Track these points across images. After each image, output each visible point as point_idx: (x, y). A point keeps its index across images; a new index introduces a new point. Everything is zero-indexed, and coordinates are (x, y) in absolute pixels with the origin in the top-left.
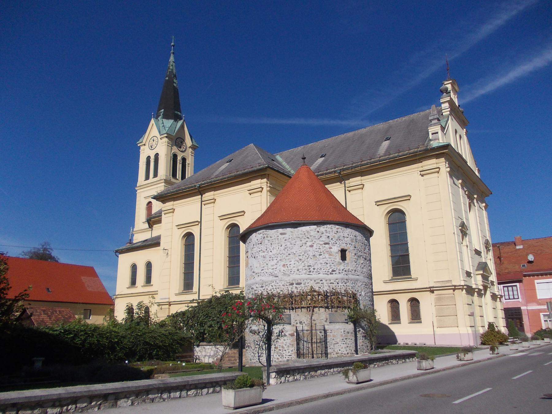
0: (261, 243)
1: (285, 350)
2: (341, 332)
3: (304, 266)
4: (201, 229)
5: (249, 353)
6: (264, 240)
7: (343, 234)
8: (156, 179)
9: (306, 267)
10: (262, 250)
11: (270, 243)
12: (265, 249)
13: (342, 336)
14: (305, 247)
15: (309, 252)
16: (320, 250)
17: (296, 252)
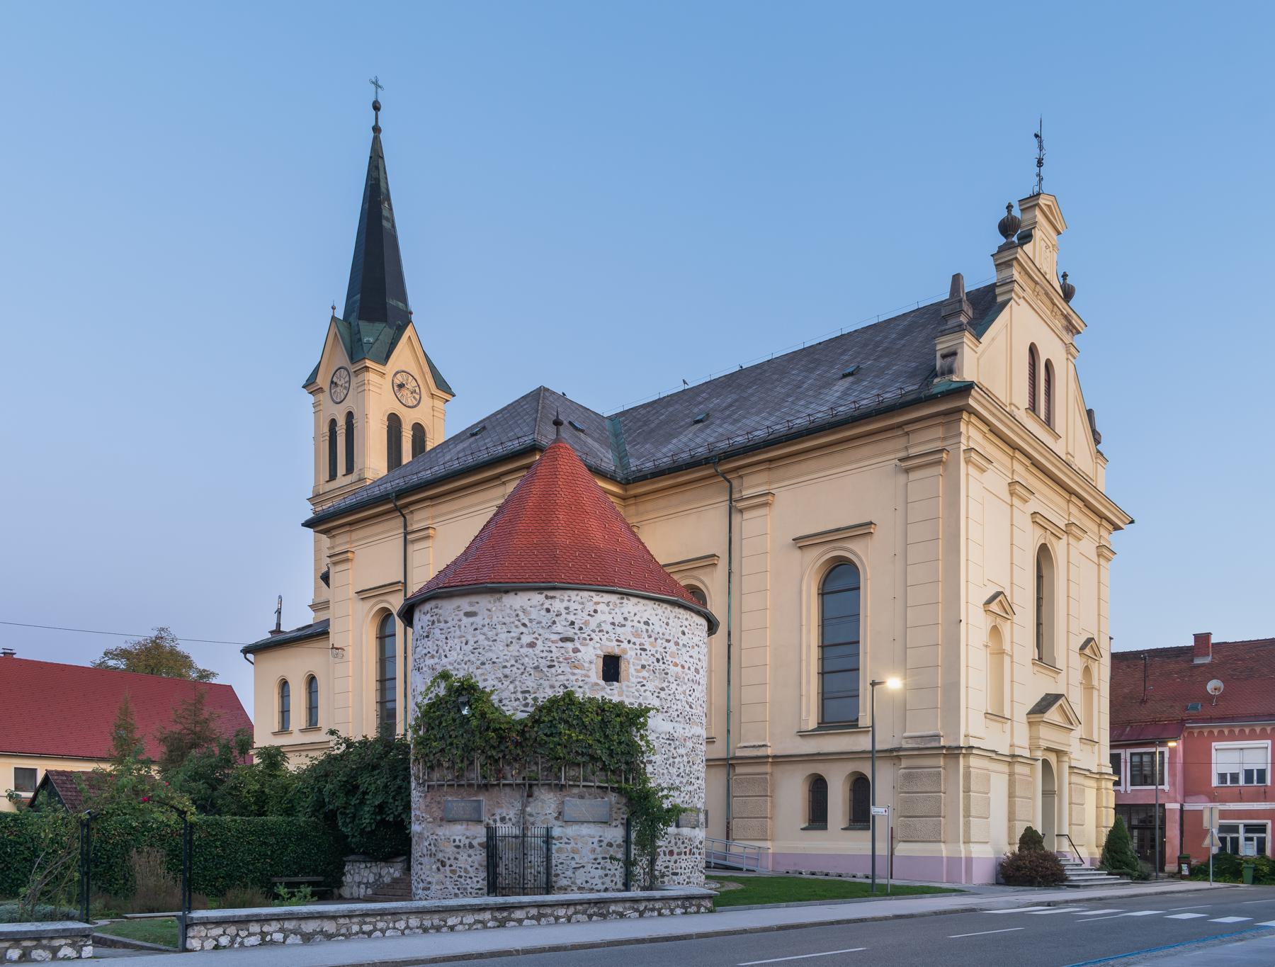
0: (427, 637)
1: (471, 878)
2: (593, 843)
3: (514, 693)
7: (612, 616)
8: (350, 479)
9: (520, 696)
11: (444, 636)
12: (434, 650)
13: (593, 851)
14: (518, 647)
15: (527, 659)
16: (549, 655)
17: (497, 658)
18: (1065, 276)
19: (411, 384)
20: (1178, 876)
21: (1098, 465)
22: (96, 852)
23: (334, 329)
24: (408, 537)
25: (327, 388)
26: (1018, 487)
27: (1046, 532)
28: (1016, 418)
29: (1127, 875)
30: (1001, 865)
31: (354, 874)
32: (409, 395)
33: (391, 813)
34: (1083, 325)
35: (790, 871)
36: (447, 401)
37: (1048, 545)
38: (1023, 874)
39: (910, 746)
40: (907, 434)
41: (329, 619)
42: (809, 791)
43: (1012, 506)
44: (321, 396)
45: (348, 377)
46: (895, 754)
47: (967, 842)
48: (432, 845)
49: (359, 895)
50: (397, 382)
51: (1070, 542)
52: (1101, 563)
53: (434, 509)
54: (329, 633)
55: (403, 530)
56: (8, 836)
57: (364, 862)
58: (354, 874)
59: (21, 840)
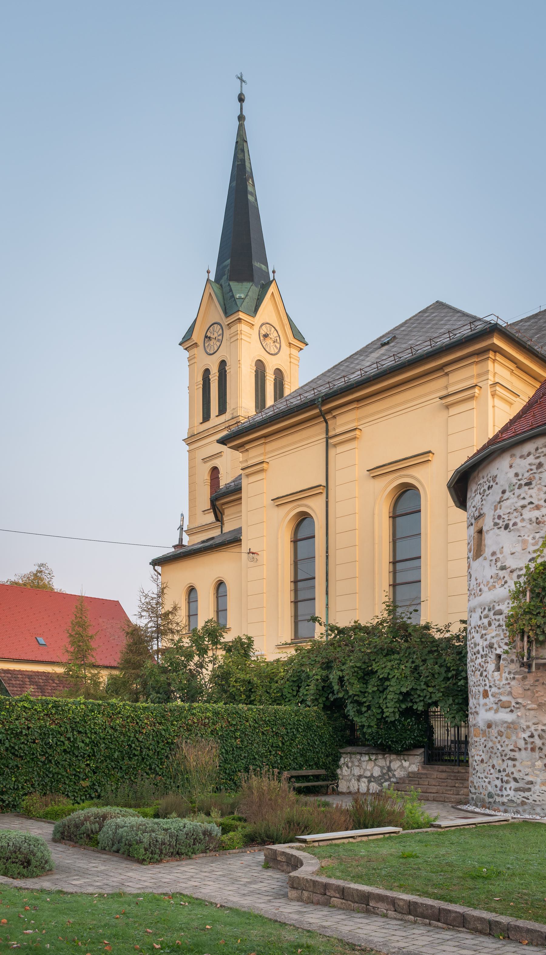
4: (327, 503)
5: (486, 778)
6: (541, 472)
8: (223, 418)
10: (531, 503)
19: (273, 335)
22: (130, 743)
23: (209, 290)
24: (330, 441)
25: (201, 343)
31: (352, 766)
32: (272, 344)
33: (421, 701)
36: (301, 349)
40: (447, 374)
41: (240, 529)
44: (195, 351)
45: (221, 331)
48: (536, 737)
49: (358, 789)
50: (263, 332)
53: (360, 411)
54: (241, 540)
55: (324, 436)
56: (50, 724)
57: (368, 754)
58: (352, 766)
59: (62, 729)
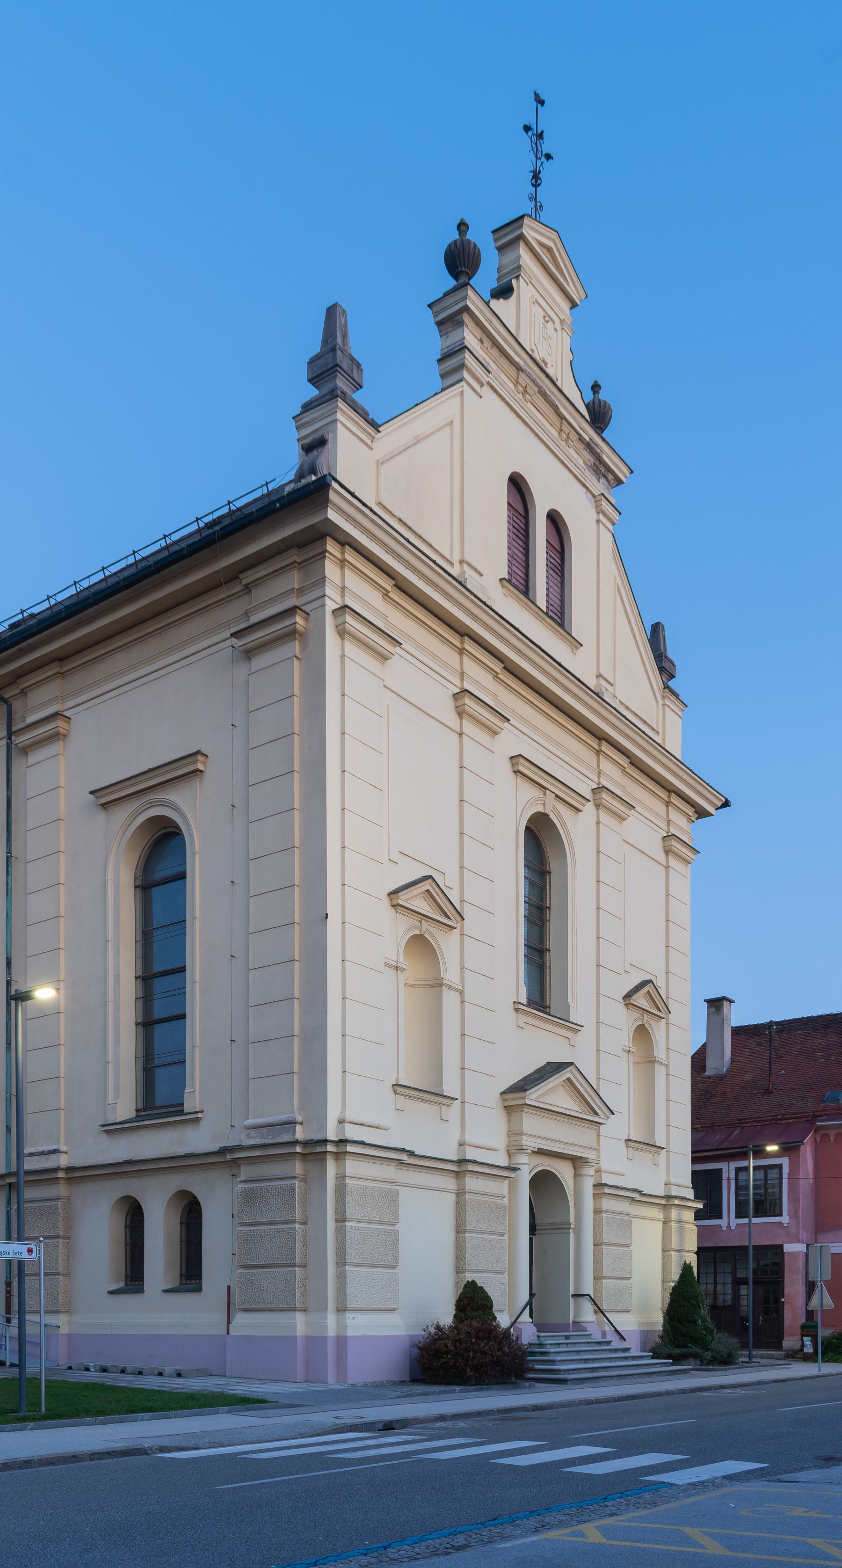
18: (596, 388)
20: (798, 1355)
21: (666, 707)
26: (468, 701)
27: (545, 794)
28: (469, 586)
29: (695, 1356)
30: (421, 1349)
34: (627, 472)
35: (74, 1367)
37: (552, 816)
38: (443, 1363)
39: (252, 1142)
40: (248, 589)
42: (126, 1226)
43: (461, 734)
46: (229, 1157)
47: (341, 1309)
51: (601, 820)
52: (670, 864)
